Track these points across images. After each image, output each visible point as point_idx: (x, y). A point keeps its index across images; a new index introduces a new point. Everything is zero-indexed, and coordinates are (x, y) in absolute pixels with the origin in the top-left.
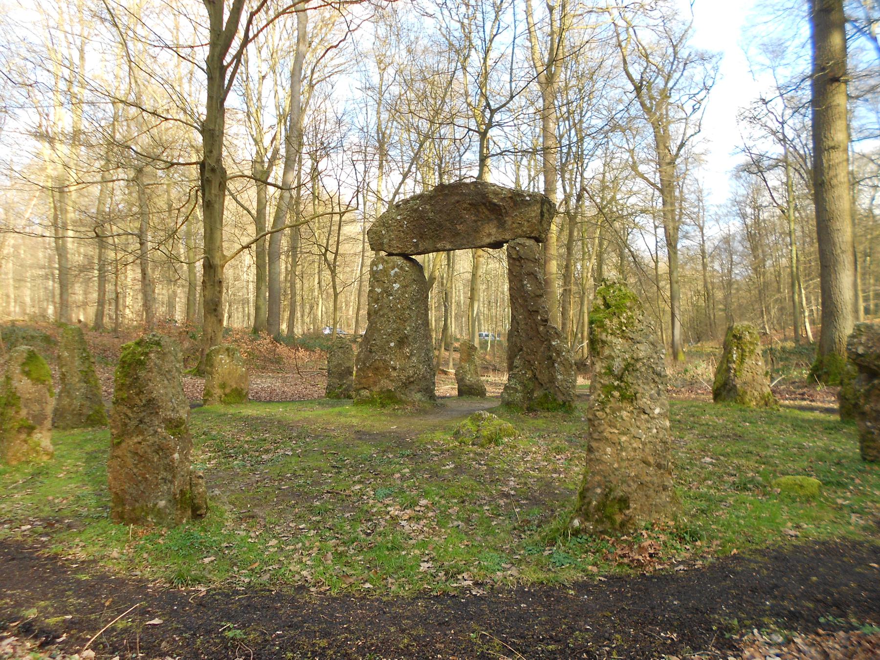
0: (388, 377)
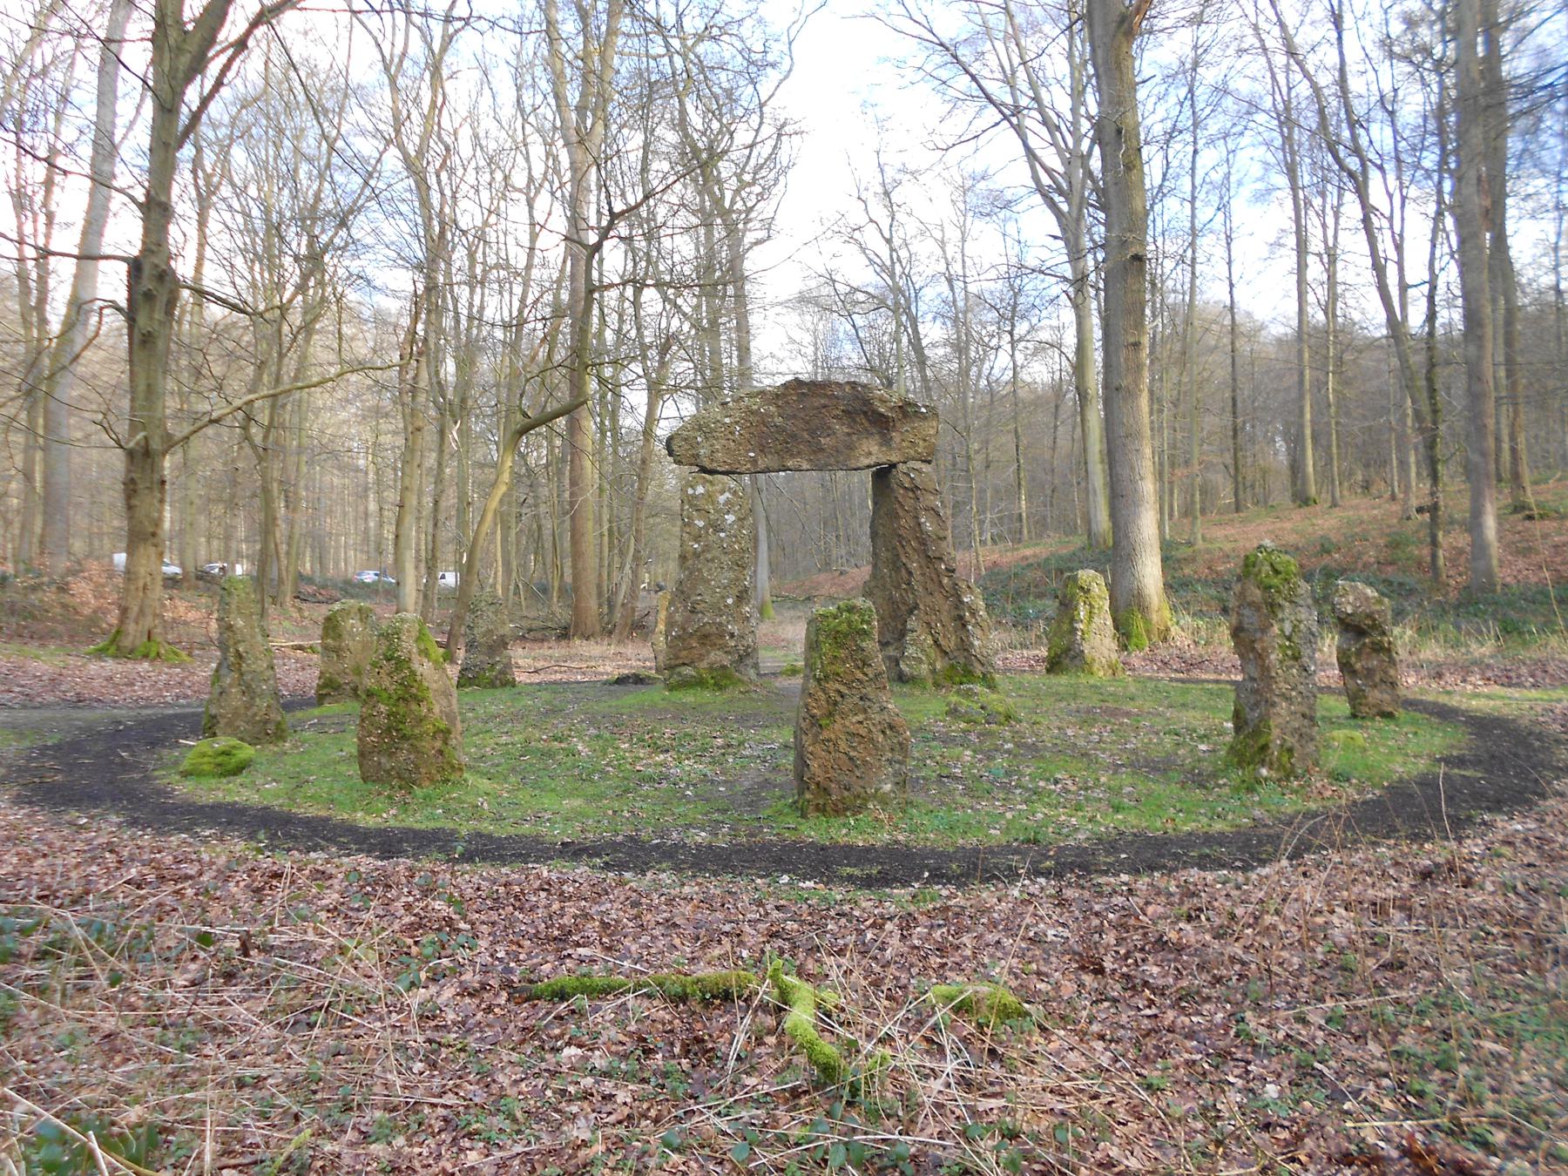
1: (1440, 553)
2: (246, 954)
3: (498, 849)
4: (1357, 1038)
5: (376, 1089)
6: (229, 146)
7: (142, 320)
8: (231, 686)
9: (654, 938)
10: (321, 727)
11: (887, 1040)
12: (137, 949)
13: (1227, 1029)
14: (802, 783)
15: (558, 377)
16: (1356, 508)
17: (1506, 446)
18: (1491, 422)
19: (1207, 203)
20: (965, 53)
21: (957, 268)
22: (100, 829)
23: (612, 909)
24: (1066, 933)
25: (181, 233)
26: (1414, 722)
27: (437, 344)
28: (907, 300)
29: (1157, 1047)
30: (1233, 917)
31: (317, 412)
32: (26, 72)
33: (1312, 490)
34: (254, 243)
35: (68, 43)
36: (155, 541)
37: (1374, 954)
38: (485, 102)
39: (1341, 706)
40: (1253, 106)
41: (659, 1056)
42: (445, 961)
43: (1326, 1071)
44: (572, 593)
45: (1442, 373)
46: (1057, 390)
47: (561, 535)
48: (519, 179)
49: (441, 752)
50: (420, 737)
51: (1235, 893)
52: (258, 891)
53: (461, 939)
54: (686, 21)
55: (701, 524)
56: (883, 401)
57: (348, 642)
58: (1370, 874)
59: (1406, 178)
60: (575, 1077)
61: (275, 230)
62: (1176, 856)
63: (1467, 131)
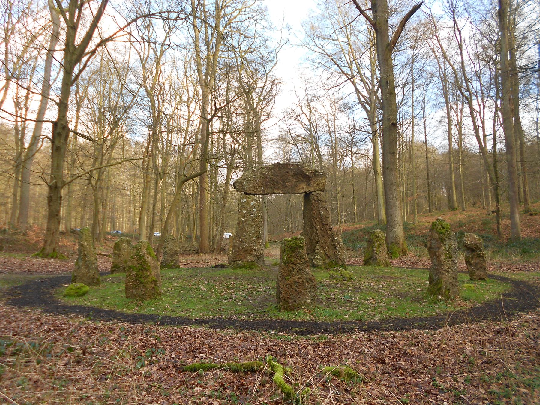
0: (252, 254)
1: (501, 227)
2: (84, 355)
3: (172, 321)
4: (475, 387)
5: (129, 400)
6: (88, 87)
7: (57, 142)
8: (82, 266)
9: (227, 351)
10: (112, 281)
11: (309, 385)
12: (47, 353)
13: (429, 383)
14: (279, 299)
15: (197, 164)
16: (471, 211)
17: (522, 190)
18: (516, 182)
19: (418, 107)
20: (335, 58)
21: (332, 129)
22: (35, 313)
23: (212, 341)
24: (372, 350)
25: (71, 114)
26: (492, 282)
27: (156, 152)
28: (316, 140)
29: (404, 389)
30: (430, 345)
31: (114, 176)
32: (21, 62)
33: (456, 205)
34: (95, 119)
35: (36, 52)
36: (57, 217)
37: (481, 358)
38: (174, 75)
39: (467, 277)
40: (433, 75)
41: (229, 390)
42: (154, 358)
43: (465, 398)
44: (200, 239)
45: (499, 165)
46: (367, 171)
47: (196, 219)
48: (185, 98)
49: (154, 288)
50: (147, 283)
51: (431, 337)
52: (89, 334)
53: (160, 351)
54: (242, 46)
55: (245, 212)
56: (308, 171)
57: (122, 252)
58: (478, 331)
59: (485, 99)
60: (199, 397)
61: (102, 114)
62: (410, 325)
63: (505, 83)
